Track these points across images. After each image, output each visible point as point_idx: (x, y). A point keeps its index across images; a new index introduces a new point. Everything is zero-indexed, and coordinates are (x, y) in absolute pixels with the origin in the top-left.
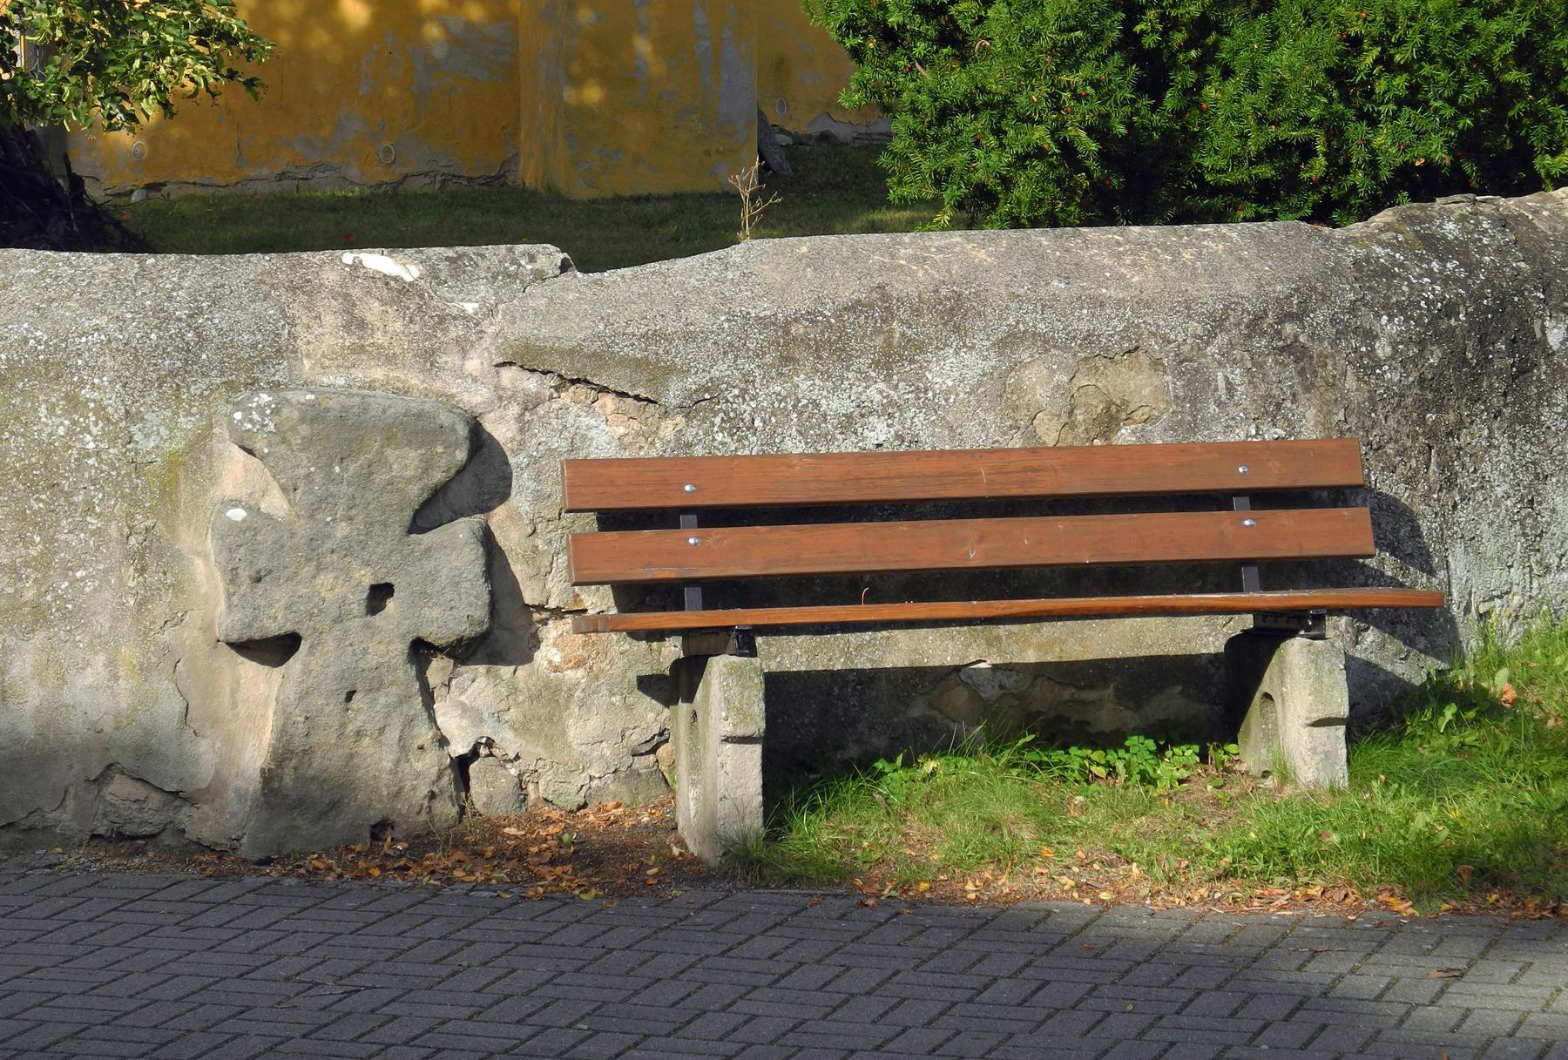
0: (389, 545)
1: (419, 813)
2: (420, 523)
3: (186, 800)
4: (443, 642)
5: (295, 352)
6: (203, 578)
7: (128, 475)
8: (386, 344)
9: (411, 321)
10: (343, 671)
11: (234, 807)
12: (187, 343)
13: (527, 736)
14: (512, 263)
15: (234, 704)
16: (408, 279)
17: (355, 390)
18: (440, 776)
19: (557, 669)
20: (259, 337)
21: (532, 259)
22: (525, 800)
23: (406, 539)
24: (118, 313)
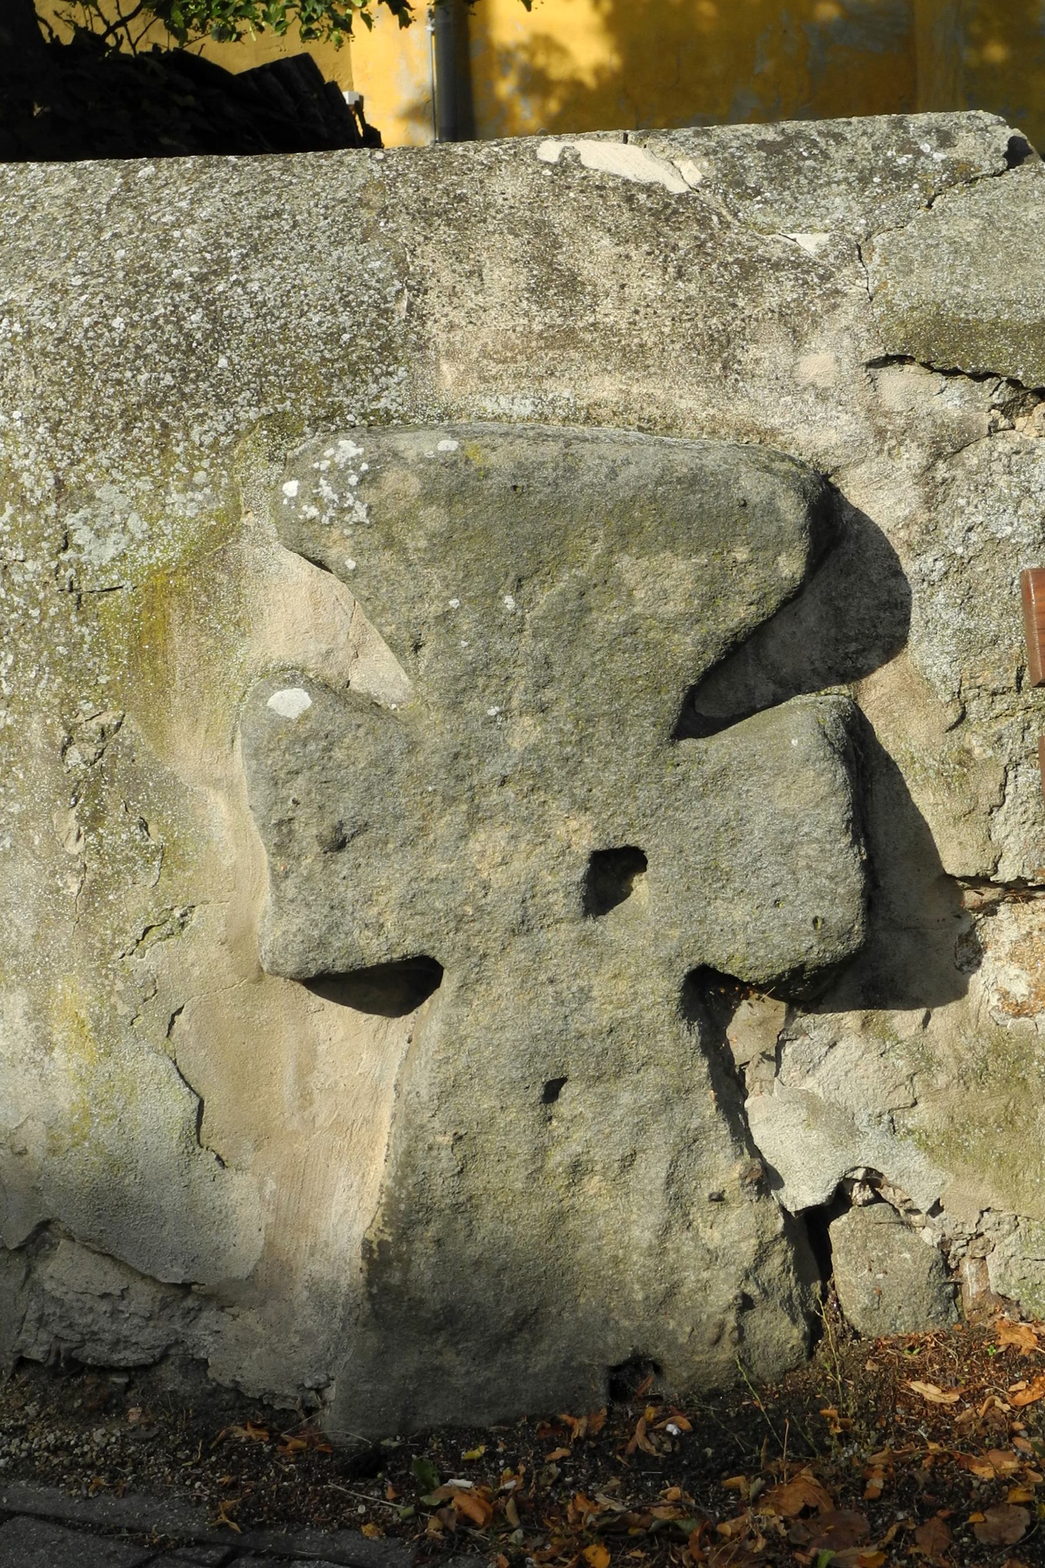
0: (632, 763)
1: (717, 1341)
2: (704, 709)
3: (207, 1298)
4: (759, 975)
5: (421, 348)
6: (227, 835)
7: (63, 616)
8: (623, 325)
9: (680, 275)
10: (535, 1038)
11: (308, 1319)
12: (189, 336)
13: (958, 1164)
14: (902, 150)
15: (305, 1098)
16: (677, 187)
17: (555, 426)
18: (762, 1255)
19: (1020, 1011)
20: (345, 318)
21: (945, 139)
22: (956, 1293)
23: (670, 752)
24: (57, 275)
